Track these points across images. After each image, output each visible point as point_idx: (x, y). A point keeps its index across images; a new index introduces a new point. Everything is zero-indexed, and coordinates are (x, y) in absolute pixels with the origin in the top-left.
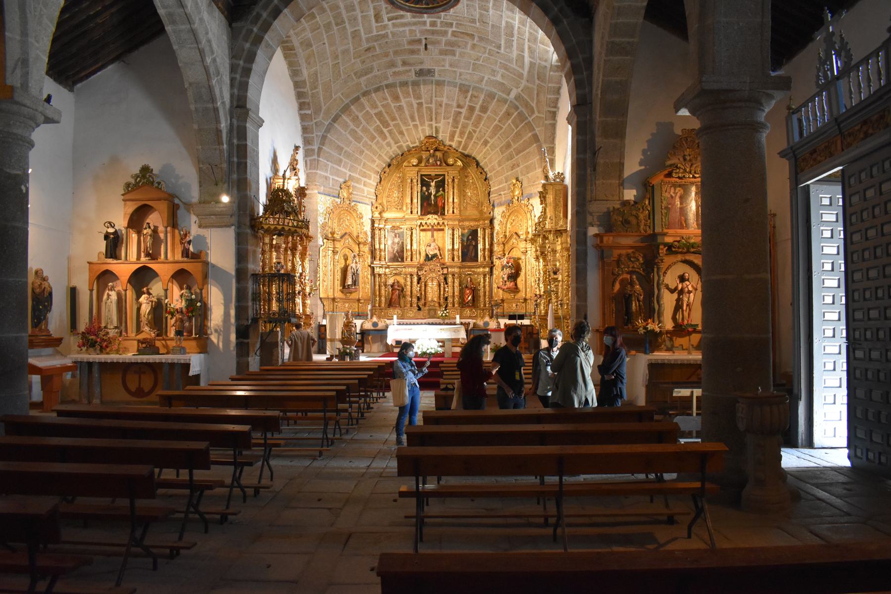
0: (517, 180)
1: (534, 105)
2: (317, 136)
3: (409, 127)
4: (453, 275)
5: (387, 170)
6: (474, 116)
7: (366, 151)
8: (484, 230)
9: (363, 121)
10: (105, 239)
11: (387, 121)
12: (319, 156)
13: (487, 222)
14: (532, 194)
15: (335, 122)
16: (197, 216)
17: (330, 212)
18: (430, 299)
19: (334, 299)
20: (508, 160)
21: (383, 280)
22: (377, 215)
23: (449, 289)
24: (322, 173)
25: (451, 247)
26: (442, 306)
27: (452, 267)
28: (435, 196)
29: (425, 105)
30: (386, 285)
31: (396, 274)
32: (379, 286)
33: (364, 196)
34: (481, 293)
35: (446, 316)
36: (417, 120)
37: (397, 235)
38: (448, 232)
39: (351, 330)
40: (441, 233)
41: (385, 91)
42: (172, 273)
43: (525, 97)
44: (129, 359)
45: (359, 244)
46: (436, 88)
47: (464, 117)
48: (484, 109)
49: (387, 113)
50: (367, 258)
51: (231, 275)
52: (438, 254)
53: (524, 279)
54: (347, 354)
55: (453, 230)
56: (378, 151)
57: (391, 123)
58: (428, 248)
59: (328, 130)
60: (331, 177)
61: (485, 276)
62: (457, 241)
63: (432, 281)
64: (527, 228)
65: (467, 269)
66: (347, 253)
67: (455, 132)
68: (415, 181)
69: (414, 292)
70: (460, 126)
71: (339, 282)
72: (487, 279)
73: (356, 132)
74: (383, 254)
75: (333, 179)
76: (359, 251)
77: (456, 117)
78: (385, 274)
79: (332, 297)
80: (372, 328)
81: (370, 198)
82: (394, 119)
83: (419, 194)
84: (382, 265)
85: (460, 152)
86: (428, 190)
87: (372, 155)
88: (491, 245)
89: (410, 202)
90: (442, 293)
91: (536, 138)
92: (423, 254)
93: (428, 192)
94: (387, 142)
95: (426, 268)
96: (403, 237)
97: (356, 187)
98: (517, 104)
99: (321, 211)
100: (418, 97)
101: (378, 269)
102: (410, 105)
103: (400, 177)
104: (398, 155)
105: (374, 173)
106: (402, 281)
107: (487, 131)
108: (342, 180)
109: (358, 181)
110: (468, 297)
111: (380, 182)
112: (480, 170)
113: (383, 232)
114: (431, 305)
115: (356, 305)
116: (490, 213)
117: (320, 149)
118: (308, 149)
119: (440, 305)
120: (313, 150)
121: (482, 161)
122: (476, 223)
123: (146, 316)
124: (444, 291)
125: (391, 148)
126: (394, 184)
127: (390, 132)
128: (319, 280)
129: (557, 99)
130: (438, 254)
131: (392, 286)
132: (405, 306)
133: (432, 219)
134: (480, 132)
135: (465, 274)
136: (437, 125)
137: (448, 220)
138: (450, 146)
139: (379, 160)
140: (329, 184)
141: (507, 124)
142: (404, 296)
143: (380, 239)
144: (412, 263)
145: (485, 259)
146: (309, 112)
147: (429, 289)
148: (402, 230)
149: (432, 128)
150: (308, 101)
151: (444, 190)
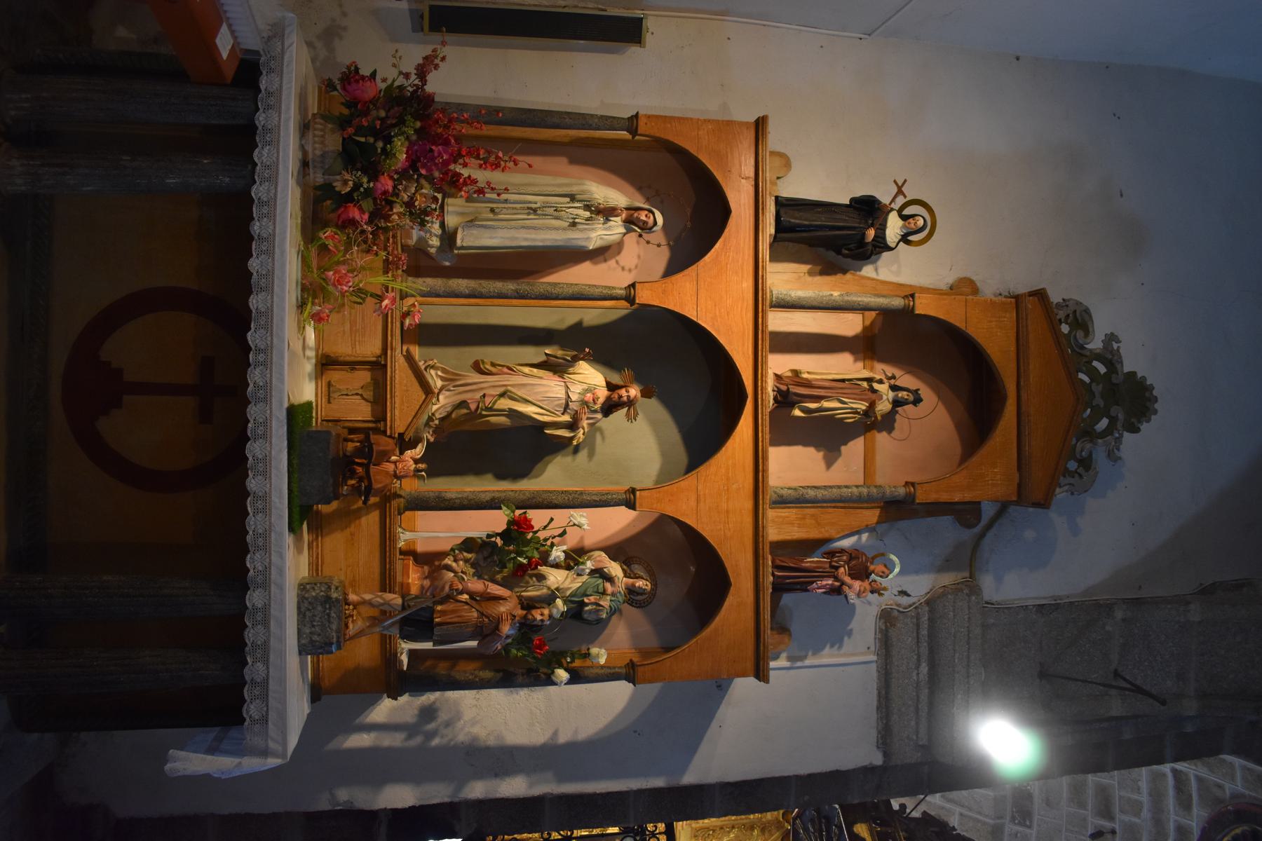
10: (855, 201)
16: (931, 602)
42: (706, 530)
44: (267, 388)
46: (984, 823)
51: (683, 769)
123: (505, 404)
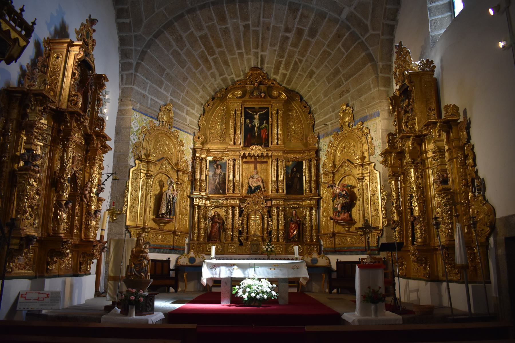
0: (347, 105)
1: (368, 23)
2: (136, 50)
3: (235, 56)
4: (278, 208)
5: (211, 102)
6: (302, 42)
7: (190, 79)
8: (310, 161)
9: (187, 43)
11: (212, 48)
12: (136, 71)
13: (313, 153)
14: (367, 116)
15: (156, 38)
17: (147, 133)
18: (253, 233)
19: (144, 229)
20: (335, 88)
21: (203, 212)
22: (198, 145)
23: (273, 223)
24: (139, 90)
25: (274, 179)
26: (265, 240)
27: (277, 199)
28: (258, 128)
29: (252, 29)
30: (205, 218)
31: (216, 207)
32: (199, 218)
33: (185, 125)
34: (308, 228)
36: (243, 48)
37: (219, 167)
38: (272, 164)
39: (141, 264)
40: (264, 165)
41: (211, 8)
43: (359, 15)
45: (178, 171)
47: (291, 44)
48: (313, 33)
49: (213, 37)
50: (187, 187)
52: (262, 186)
53: (361, 208)
54: (131, 303)
55: (277, 161)
56: (202, 81)
57: (217, 50)
58: (251, 180)
59: (148, 46)
60: (150, 97)
61: (311, 209)
62: (281, 172)
63: (255, 214)
64: (363, 153)
65: (292, 202)
66: (164, 180)
67: (280, 62)
68: (238, 112)
69: (236, 225)
70: (286, 55)
71: (152, 210)
72: (314, 211)
73: (179, 54)
74: (203, 185)
75: (151, 99)
76: (178, 179)
77: (283, 44)
78: (205, 206)
79: (142, 226)
80: (188, 264)
81: (192, 128)
82: (219, 46)
83: (243, 126)
84: (202, 196)
85: (284, 87)
86: (251, 122)
87: (196, 84)
88: (318, 176)
89: (233, 133)
90: (265, 226)
91: (370, 58)
92: (246, 187)
93: (252, 124)
94: (212, 73)
95: (249, 200)
96: (226, 168)
97: (177, 113)
98: (349, 24)
99: (135, 129)
100: (245, 18)
102: (236, 28)
103: (223, 110)
104: (223, 88)
105: (198, 104)
106: (223, 214)
107: (314, 59)
108: (162, 103)
109: (181, 108)
110: (294, 231)
111: (204, 114)
112: (304, 104)
113: (204, 162)
114: (254, 240)
115: (171, 238)
116: (315, 145)
117: (138, 64)
118: (125, 63)
119: (263, 240)
120: (131, 64)
121: (306, 95)
122: (301, 155)
124: (268, 224)
125: (216, 80)
126: (217, 116)
127: (215, 60)
128: (127, 205)
129: (397, 11)
130: (262, 186)
131: (213, 218)
132: (226, 240)
133: (256, 150)
134: (306, 61)
135: (289, 208)
136: (262, 53)
137: (273, 151)
138: (275, 80)
139: (203, 91)
140: (147, 103)
141: (337, 47)
142: (225, 230)
143: (201, 169)
144: (234, 195)
145: (311, 191)
146: (127, 21)
147: (252, 223)
148: (224, 162)
149: (257, 57)
150: (126, 7)
151: (268, 123)
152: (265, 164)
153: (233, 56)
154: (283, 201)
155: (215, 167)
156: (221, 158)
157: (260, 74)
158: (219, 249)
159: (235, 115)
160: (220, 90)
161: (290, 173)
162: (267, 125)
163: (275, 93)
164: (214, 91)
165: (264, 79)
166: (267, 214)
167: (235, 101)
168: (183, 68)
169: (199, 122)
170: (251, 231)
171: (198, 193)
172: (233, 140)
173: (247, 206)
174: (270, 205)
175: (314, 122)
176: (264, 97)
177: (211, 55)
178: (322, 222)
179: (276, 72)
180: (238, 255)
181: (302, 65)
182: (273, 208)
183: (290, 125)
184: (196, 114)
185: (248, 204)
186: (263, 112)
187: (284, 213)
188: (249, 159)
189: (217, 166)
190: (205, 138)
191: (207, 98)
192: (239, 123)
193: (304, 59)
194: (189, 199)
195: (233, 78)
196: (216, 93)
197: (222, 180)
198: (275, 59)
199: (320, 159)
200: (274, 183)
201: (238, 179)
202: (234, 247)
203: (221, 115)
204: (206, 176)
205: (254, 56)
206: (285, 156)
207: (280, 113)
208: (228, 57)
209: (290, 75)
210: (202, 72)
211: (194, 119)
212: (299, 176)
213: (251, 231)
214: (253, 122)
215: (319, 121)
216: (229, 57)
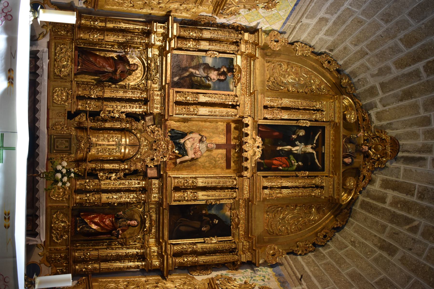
3: (421, 111)
4: (144, 190)
7: (385, 26)
18: (94, 140)
25: (200, 183)
27: (161, 189)
28: (290, 152)
30: (123, 45)
33: (303, 15)
35: (56, 181)
37: (222, 78)
52: (186, 158)
55: (233, 188)
56: (377, 51)
58: (197, 137)
61: (141, 257)
62: (211, 196)
63: (132, 145)
65: (154, 216)
67: (409, 191)
68: (318, 116)
69: (109, 107)
70: (425, 203)
72: (137, 263)
74: (191, 44)
78: (148, 46)
81: (295, 28)
83: (294, 123)
86: (301, 139)
87: (373, 38)
90: (107, 166)
92: (182, 127)
93: (296, 140)
95: (159, 133)
96: (219, 89)
101: (161, 31)
103: (319, 89)
104: (356, 89)
105: (333, 42)
107: (419, 255)
110: (96, 224)
113: (233, 47)
114: (79, 142)
119: (78, 162)
121: (345, 238)
124: (111, 171)
125: (373, 76)
126: (310, 78)
127: (416, 74)
130: (186, 158)
131: (123, 60)
135: (144, 213)
136: (429, 161)
138: (371, 181)
142: (100, 83)
144: (171, 104)
148: (231, 87)
149: (419, 151)
151: (299, 169)
152: (224, 165)
153: (421, 108)
154: (157, 199)
155: (222, 70)
156: (239, 80)
157: (384, 155)
158: (60, 71)
159: (314, 110)
160: (353, 83)
161: (209, 212)
162: (295, 167)
163: (351, 183)
164: (351, 72)
165: (374, 163)
166: (132, 168)
167: (337, 110)
168: (410, 14)
169: (302, 43)
170: (98, 137)
171: (175, 33)
172: (272, 104)
173: (149, 130)
174: (149, 175)
175: (300, 255)
176: (344, 163)
177: (426, 68)
178: (115, 282)
179: (386, 184)
180: (48, 110)
181: (405, 232)
182: (143, 180)
183: (293, 210)
184: (317, 38)
185: (153, 132)
186: (317, 161)
187: (133, 203)
188: (234, 134)
189: (224, 73)
190: (275, 54)
191: (341, 60)
192: (301, 117)
193: (418, 237)
194: (164, 13)
195: (376, 107)
196: (348, 76)
197: (197, 81)
198: (417, 184)
199: (236, 270)
200: (193, 182)
201: (200, 113)
202: (65, 101)
203: (311, 85)
204: (206, 51)
205: (424, 145)
206: (241, 202)
207: (317, 192)
208: (420, 99)
209: (384, 208)
210: (395, 50)
211: (309, 34)
212: (204, 229)
213: (98, 137)
214: (300, 142)
215: (303, 263)
216: (420, 100)
